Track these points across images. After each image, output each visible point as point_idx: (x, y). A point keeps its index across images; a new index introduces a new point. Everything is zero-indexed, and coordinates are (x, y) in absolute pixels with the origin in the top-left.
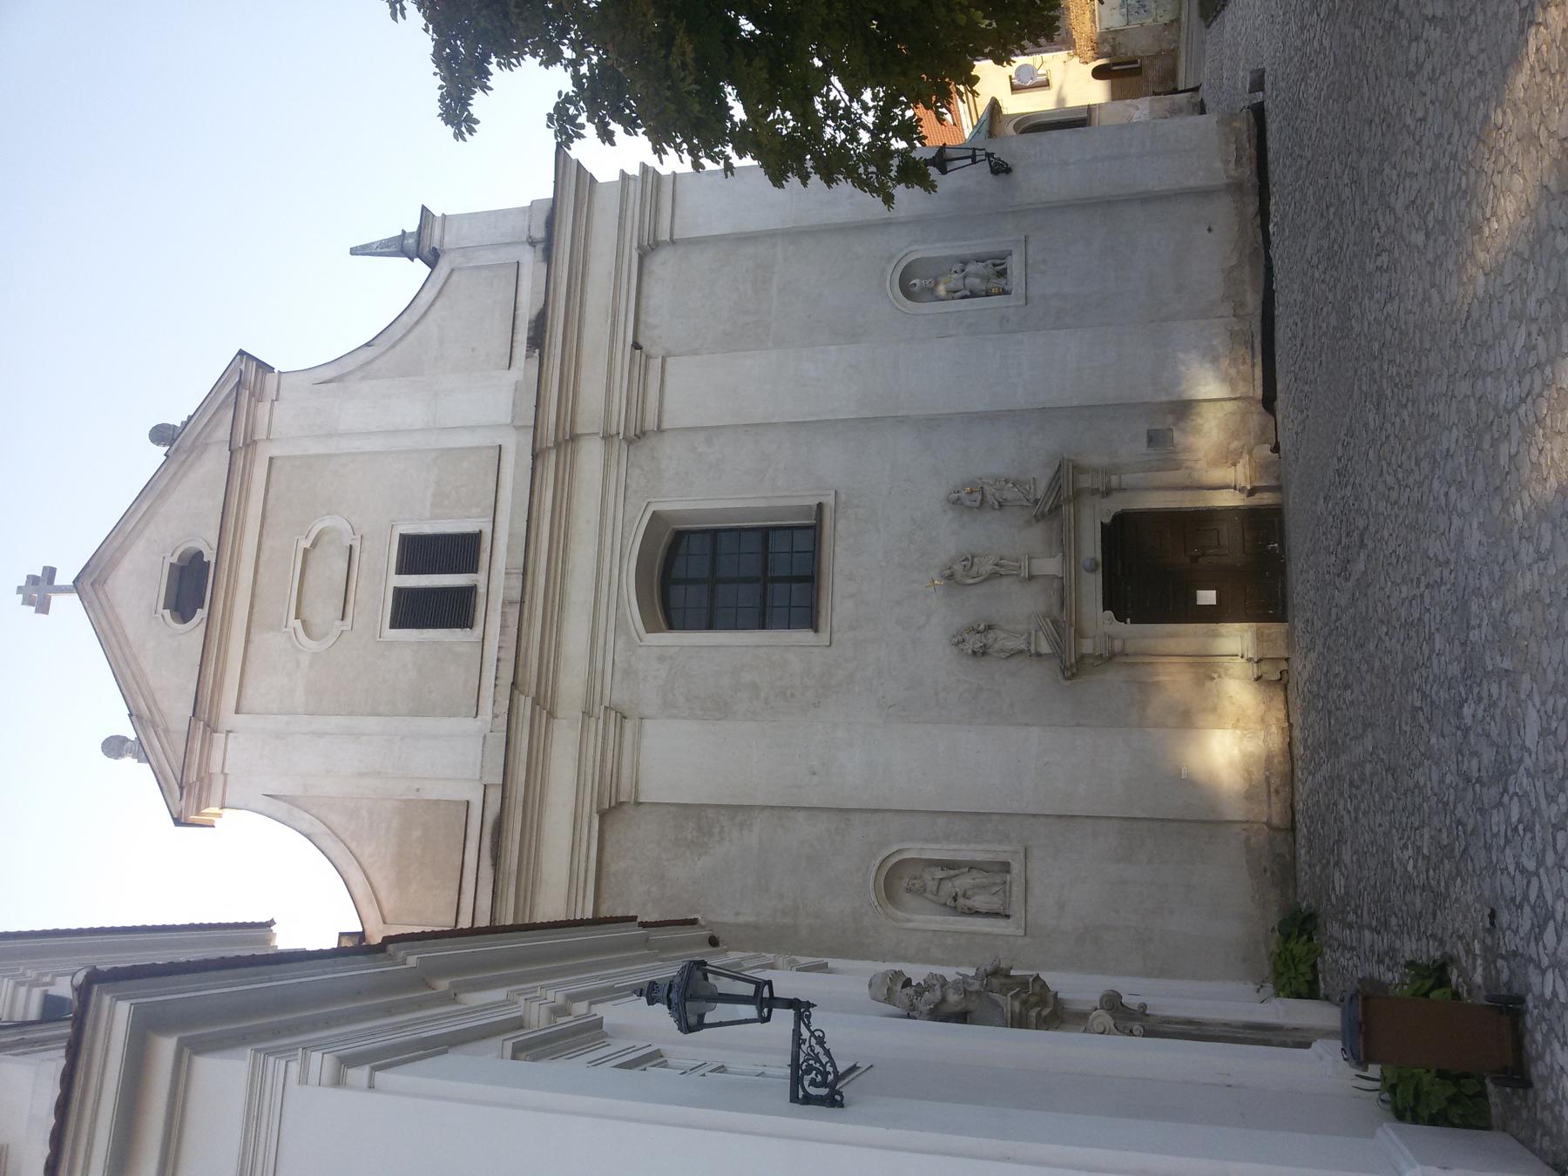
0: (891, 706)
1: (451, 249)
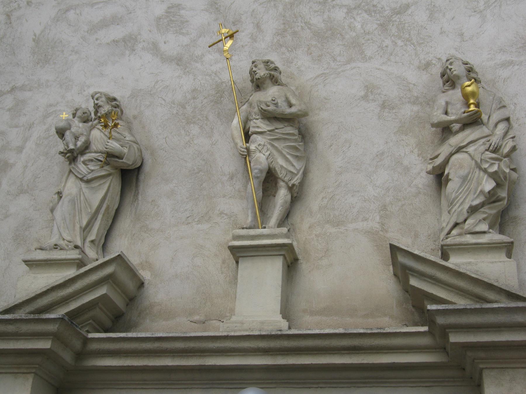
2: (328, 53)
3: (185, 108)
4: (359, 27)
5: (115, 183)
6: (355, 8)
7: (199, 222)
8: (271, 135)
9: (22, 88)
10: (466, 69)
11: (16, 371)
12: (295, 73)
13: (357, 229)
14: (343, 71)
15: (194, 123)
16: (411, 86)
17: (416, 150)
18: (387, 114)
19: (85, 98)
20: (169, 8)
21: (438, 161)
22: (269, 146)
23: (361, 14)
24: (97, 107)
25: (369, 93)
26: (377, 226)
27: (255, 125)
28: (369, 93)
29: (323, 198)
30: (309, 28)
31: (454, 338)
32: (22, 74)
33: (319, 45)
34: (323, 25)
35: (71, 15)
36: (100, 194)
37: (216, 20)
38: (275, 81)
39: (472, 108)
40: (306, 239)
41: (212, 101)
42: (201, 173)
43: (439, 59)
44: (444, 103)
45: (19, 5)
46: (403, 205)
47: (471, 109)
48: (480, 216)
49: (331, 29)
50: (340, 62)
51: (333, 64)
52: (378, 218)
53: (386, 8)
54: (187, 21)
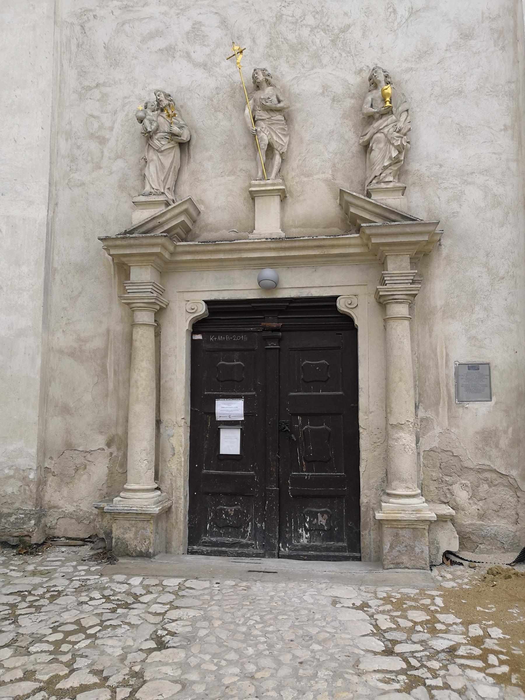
0: (83, 27)
1: (367, 672)
2: (299, 62)
3: (213, 101)
4: (319, 42)
5: (177, 151)
6: (316, 28)
7: (228, 175)
8: (269, 121)
9: (104, 84)
10: (384, 75)
11: (140, 264)
12: (279, 76)
13: (319, 178)
14: (309, 75)
15: (219, 111)
16: (350, 85)
17: (352, 129)
18: (336, 105)
19: (148, 93)
20: (193, 24)
21: (367, 138)
22: (268, 129)
23: (319, 32)
24: (159, 101)
25: (325, 91)
26: (330, 176)
27: (259, 114)
28: (325, 91)
29: (299, 160)
30: (287, 43)
31: (374, 240)
32: (102, 74)
33: (294, 56)
34: (295, 41)
35: (127, 27)
36: (170, 160)
37: (226, 35)
38: (269, 83)
39: (388, 104)
40: (291, 185)
41: (229, 96)
42: (227, 145)
43: (368, 66)
44: (370, 100)
45: (88, 18)
46: (344, 164)
47: (386, 105)
48: (388, 171)
49: (300, 44)
50: (306, 68)
51: (302, 70)
52: (330, 172)
53: (336, 28)
54: (207, 36)
